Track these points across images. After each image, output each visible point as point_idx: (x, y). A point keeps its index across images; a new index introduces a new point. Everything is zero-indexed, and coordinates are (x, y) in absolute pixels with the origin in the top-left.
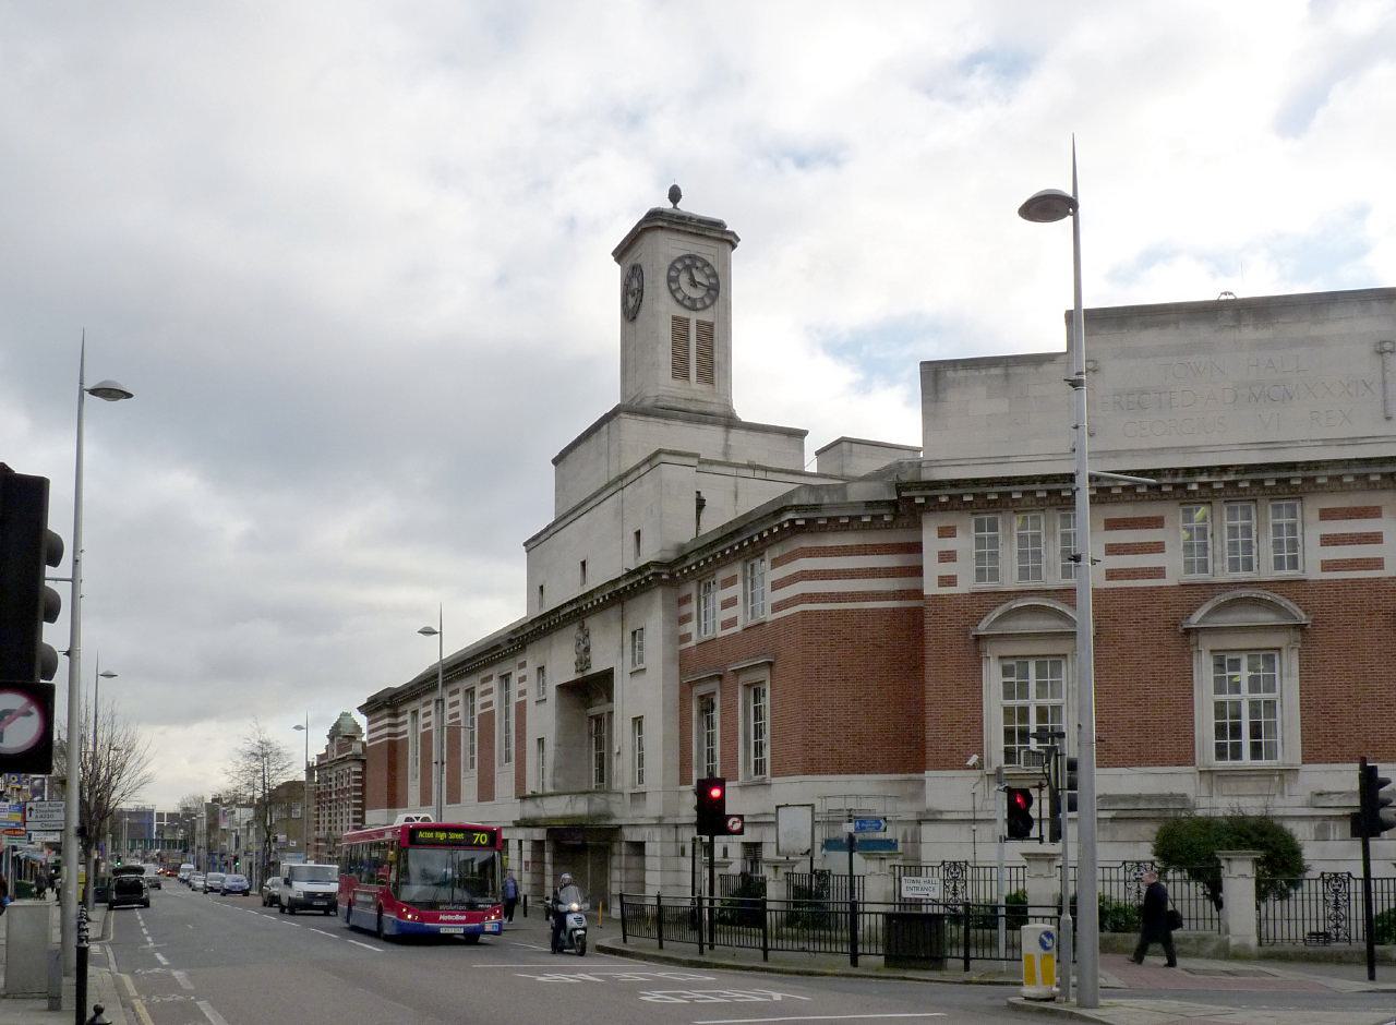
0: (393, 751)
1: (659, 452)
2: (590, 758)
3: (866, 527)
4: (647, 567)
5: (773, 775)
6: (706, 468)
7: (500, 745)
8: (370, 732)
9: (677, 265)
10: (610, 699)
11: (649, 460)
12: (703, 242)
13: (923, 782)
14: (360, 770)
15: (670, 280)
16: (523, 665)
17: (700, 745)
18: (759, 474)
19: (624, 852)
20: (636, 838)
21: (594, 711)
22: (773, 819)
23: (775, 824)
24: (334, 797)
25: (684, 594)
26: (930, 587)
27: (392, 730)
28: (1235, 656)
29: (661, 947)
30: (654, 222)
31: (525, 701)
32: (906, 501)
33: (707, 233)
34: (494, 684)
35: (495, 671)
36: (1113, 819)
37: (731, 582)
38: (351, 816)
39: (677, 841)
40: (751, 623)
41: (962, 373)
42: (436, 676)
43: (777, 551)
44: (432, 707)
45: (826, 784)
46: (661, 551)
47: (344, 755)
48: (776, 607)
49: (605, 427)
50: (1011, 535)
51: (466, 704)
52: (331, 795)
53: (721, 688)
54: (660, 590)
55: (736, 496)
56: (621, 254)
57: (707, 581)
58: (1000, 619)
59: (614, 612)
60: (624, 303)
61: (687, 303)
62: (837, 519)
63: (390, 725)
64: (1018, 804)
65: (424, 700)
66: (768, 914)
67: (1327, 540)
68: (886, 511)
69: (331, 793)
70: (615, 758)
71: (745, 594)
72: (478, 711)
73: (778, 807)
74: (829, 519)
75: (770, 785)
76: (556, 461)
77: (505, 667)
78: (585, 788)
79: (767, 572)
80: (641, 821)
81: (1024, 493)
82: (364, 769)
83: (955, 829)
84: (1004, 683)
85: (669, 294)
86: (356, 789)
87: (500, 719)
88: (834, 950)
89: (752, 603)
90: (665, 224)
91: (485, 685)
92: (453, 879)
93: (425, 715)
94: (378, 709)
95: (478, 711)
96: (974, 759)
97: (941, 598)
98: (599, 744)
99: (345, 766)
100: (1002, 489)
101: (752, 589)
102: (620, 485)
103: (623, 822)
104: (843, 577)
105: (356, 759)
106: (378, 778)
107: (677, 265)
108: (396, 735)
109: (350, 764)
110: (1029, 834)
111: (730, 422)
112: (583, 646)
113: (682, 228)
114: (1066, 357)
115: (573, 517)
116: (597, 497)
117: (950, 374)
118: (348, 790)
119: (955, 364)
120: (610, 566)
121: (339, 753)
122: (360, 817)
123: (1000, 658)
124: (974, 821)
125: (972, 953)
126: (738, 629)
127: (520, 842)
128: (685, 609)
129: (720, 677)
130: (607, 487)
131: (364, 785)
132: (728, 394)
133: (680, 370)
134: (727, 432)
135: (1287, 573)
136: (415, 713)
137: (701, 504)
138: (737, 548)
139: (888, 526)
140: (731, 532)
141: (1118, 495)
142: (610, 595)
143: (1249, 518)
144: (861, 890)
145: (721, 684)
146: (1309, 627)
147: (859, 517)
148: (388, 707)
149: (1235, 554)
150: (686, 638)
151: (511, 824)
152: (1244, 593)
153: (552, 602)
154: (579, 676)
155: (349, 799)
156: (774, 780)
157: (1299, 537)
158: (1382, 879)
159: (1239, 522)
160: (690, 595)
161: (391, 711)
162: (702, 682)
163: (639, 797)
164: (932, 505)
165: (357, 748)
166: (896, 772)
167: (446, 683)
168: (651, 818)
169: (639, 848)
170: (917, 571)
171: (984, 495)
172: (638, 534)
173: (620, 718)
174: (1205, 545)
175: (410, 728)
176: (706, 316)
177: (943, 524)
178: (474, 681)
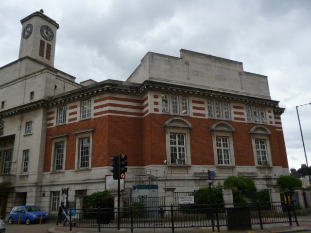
9: (40, 30)
10: (13, 145)
15: (48, 27)
20: (22, 190)
23: (105, 182)
28: (220, 138)
36: (199, 180)
39: (41, 191)
40: (82, 119)
41: (159, 57)
48: (95, 114)
53: (93, 136)
55: (64, 87)
58: (170, 122)
59: (17, 117)
62: (121, 90)
70: (13, 164)
73: (106, 176)
74: (119, 89)
92: (152, 220)
104: (123, 107)
115: (12, 84)
119: (157, 54)
123: (170, 133)
124: (166, 180)
126: (78, 120)
129: (67, 136)
132: (53, 64)
141: (196, 94)
145: (93, 134)
158: (180, 193)
166: (136, 166)
168: (33, 183)
176: (50, 43)
177: (155, 94)
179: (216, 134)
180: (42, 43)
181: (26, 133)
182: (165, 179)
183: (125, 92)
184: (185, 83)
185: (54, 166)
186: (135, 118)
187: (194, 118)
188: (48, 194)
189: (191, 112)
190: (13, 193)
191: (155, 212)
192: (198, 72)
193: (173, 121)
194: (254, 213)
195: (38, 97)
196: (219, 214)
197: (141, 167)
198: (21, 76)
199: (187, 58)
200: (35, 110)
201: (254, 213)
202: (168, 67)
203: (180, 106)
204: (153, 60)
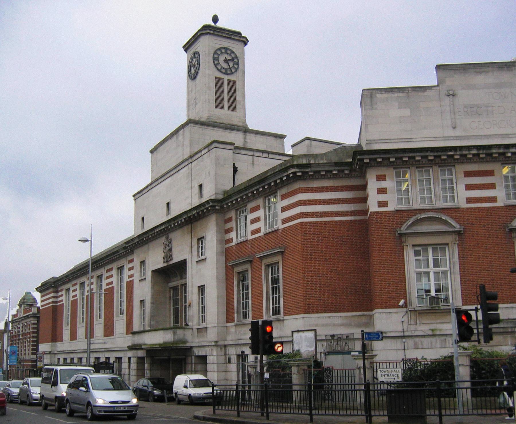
0: (55, 311)
1: (214, 141)
2: (170, 310)
3: (335, 177)
4: (207, 202)
5: (285, 315)
6: (238, 151)
7: (117, 305)
8: (42, 301)
9: (217, 53)
11: (208, 146)
12: (229, 41)
13: (371, 317)
14: (36, 322)
15: (226, 49)
16: (131, 261)
17: (239, 301)
18: (265, 155)
19: (194, 362)
21: (172, 284)
22: (290, 339)
23: (292, 342)
24: (21, 337)
25: (228, 216)
26: (373, 207)
27: (55, 300)
29: (239, 415)
30: (207, 30)
31: (133, 280)
32: (354, 164)
33: (232, 37)
34: (114, 272)
35: (115, 265)
37: (256, 209)
38: (31, 348)
39: (225, 355)
40: (269, 230)
41: (385, 95)
42: (88, 266)
43: (284, 191)
44: (77, 287)
45: (317, 319)
46: (216, 194)
47: (28, 314)
48: (284, 221)
49: (181, 132)
50: (415, 179)
51: (97, 283)
52: (19, 336)
54: (215, 215)
56: (187, 47)
57: (241, 210)
58: (413, 224)
59: (187, 228)
60: (189, 71)
61: (223, 71)
63: (53, 297)
64: (463, 320)
65: (109, 267)
66: (293, 392)
67: (469, 187)
68: (347, 168)
69: (19, 335)
71: (265, 215)
72: (104, 287)
73: (293, 332)
74: (315, 172)
75: (283, 320)
76: (152, 152)
77: (120, 263)
78: (168, 326)
79: (278, 203)
80: (205, 344)
81: (422, 157)
82: (38, 321)
83: (394, 341)
84: (416, 260)
85: (214, 66)
86: (33, 333)
87: (117, 290)
88: (292, 412)
89: (269, 220)
90: (212, 32)
91: (108, 273)
93: (73, 291)
94: (47, 289)
95: (104, 287)
96: (402, 302)
97: (381, 213)
98: (175, 303)
99: (28, 320)
100: (411, 155)
101: (269, 212)
102: (190, 161)
103: (193, 345)
105: (34, 316)
106: (46, 326)
107: (217, 53)
108: (56, 302)
109: (31, 319)
110: (470, 339)
111: (246, 131)
112: (168, 248)
113: (220, 34)
114: (438, 88)
116: (177, 168)
117: (379, 95)
118: (29, 333)
119: (381, 90)
120: (184, 202)
121: (24, 314)
122: (35, 347)
123: (414, 246)
124: (404, 337)
125: (443, 412)
126: (261, 234)
127: (130, 358)
128: (228, 226)
129: (251, 262)
130: (183, 162)
131: (38, 330)
133: (219, 104)
134: (245, 135)
135: (450, 204)
136: (68, 290)
137: (235, 170)
138: (261, 190)
139: (348, 176)
140: (251, 185)
142: (185, 219)
143: (452, 175)
144: (353, 378)
146: (462, 232)
147: (331, 171)
148: (53, 287)
149: (446, 193)
150: (230, 240)
151: (127, 349)
152: (431, 215)
153: (150, 225)
154: (165, 265)
155: (29, 338)
156: (286, 318)
157: (455, 186)
159: (447, 177)
160: (231, 217)
161: (54, 290)
162: (238, 264)
163: (202, 331)
164: (374, 164)
165: (34, 310)
166: (356, 311)
167: (93, 270)
168: (211, 342)
169: (203, 359)
170: (364, 200)
171: (401, 158)
172: (201, 186)
173: (190, 287)
174: (453, 187)
175: (64, 299)
176: (232, 78)
177: (380, 173)
178: (102, 271)
179: (411, 241)
180: (219, 82)
181: (141, 276)
182: (402, 334)
183: (328, 175)
184: (445, 138)
185: (239, 313)
186: (355, 221)
187: (468, 209)
188: (234, 359)
189: (462, 196)
190: (192, 356)
191: (347, 392)
192: (478, 106)
193: (413, 224)
194: (445, 401)
195: (209, 194)
196: (442, 399)
197: (366, 313)
198: (186, 157)
199: (454, 81)
200: (206, 216)
201: (445, 401)
202: (406, 112)
203: (437, 188)
204: (372, 105)
